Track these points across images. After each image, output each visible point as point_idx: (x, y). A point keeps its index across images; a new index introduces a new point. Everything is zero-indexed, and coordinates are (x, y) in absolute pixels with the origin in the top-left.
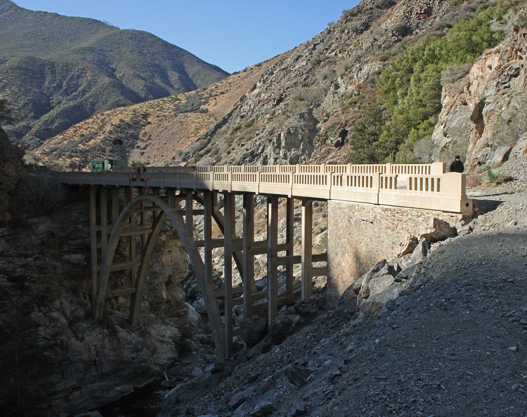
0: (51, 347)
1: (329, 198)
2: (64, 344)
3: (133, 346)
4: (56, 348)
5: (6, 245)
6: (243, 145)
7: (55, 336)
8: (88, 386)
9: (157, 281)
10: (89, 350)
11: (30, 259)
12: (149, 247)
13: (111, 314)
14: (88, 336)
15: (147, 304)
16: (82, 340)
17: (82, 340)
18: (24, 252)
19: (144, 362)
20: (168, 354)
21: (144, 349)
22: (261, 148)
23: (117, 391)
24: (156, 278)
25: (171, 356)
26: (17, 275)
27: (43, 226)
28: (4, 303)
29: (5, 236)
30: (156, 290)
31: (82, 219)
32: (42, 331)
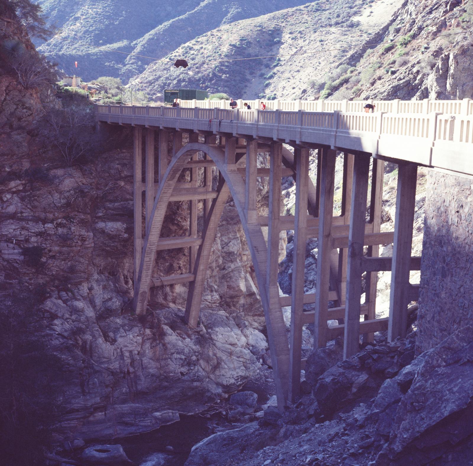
0: (68, 349)
1: (428, 164)
2: (88, 346)
3: (183, 357)
4: (76, 350)
5: (19, 204)
6: (393, 73)
7: (77, 332)
8: (116, 406)
9: (233, 266)
10: (122, 356)
11: (50, 225)
12: (213, 218)
13: (163, 307)
14: (121, 337)
15: (216, 296)
16: (113, 341)
17: (113, 341)
18: (43, 215)
19: (198, 381)
20: (237, 370)
21: (201, 362)
22: (419, 77)
23: (156, 418)
24: (232, 262)
25: (243, 374)
26: (31, 246)
27: (69, 181)
28: (11, 284)
29: (19, 191)
30: (231, 278)
31: (125, 173)
32: (58, 326)
